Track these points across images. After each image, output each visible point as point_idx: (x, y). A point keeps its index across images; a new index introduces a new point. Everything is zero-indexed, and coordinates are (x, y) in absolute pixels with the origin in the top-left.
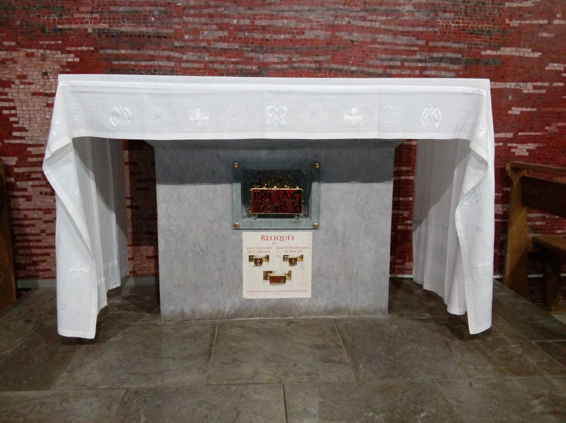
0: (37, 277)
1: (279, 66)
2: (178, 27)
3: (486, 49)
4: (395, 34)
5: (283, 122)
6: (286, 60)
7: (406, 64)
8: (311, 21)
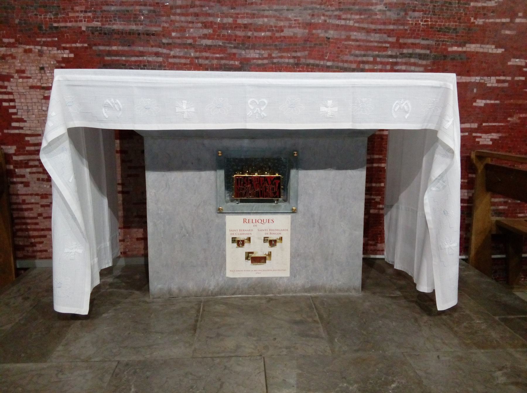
1: (260, 62)
2: (166, 25)
3: (452, 45)
4: (368, 31)
5: (263, 113)
6: (266, 55)
7: (378, 59)
8: (290, 20)
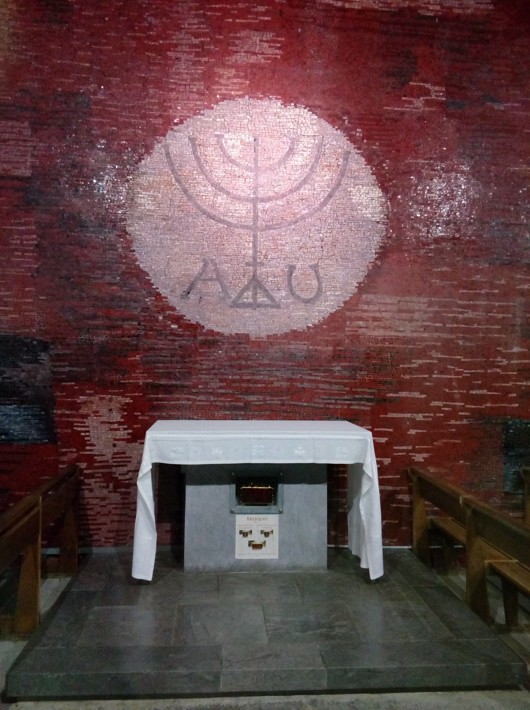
0: (91, 545)
1: (258, 403)
2: (195, 381)
3: (389, 393)
4: (330, 383)
5: (262, 454)
6: (262, 399)
7: (338, 402)
8: (278, 377)
